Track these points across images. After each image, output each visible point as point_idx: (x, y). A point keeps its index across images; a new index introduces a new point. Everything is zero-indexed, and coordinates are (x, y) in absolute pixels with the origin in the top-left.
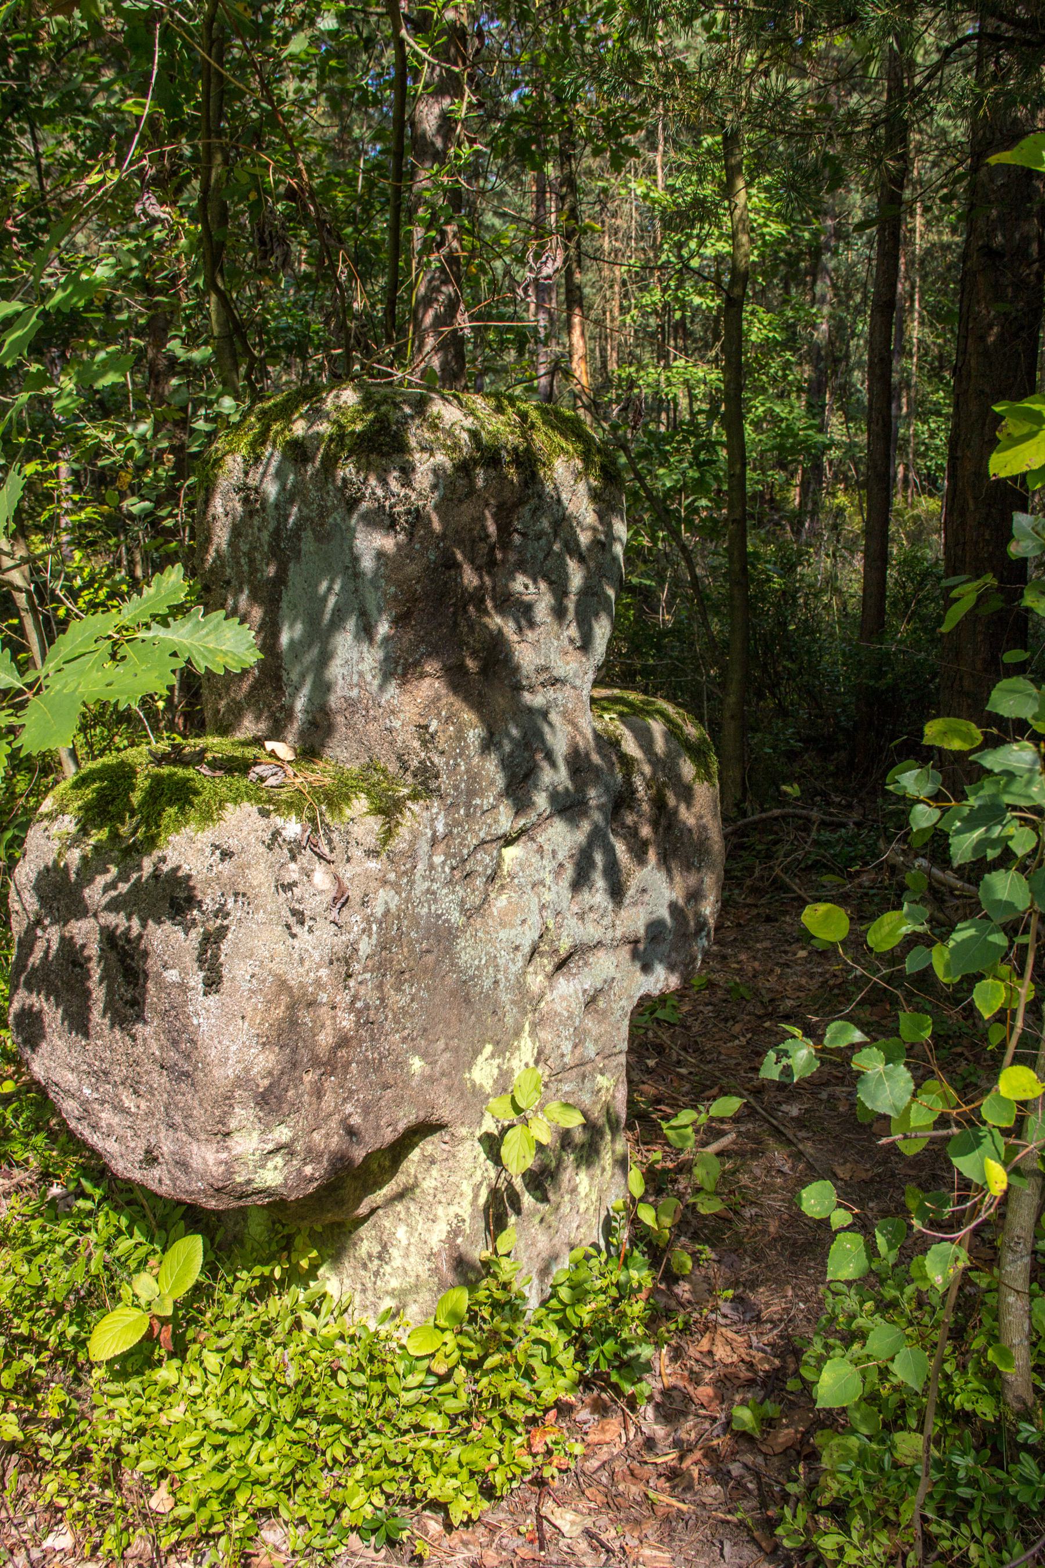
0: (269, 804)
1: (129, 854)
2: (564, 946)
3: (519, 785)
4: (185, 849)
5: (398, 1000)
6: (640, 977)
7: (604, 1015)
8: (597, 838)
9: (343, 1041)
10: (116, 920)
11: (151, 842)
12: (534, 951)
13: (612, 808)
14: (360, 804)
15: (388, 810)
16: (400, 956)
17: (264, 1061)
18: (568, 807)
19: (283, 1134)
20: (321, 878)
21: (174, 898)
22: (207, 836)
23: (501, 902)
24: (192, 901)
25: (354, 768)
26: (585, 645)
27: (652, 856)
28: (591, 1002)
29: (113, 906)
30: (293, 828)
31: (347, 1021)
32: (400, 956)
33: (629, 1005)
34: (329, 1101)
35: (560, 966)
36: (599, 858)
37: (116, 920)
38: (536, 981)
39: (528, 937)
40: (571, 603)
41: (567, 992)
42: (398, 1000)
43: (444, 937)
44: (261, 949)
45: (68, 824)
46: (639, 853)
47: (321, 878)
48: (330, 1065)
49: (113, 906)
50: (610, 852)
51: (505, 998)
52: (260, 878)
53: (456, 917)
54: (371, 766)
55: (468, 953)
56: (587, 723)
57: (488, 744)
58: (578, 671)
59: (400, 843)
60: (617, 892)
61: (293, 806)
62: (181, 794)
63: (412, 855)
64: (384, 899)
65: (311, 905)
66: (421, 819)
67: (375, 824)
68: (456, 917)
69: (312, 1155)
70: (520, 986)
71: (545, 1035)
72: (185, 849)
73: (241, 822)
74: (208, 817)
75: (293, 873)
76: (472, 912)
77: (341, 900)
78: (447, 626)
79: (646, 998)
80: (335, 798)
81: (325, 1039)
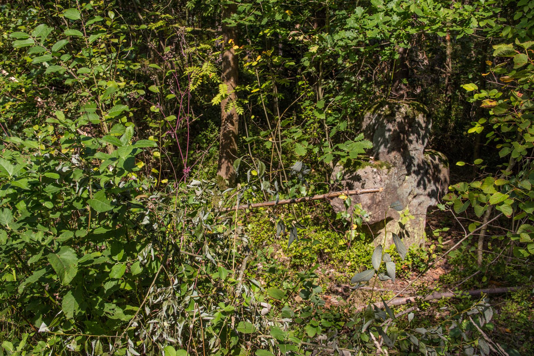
0: (372, 166)
1: (352, 172)
2: (415, 193)
3: (409, 168)
4: (360, 172)
5: (388, 197)
6: (429, 202)
7: (422, 207)
8: (422, 179)
9: (380, 201)
10: (349, 181)
11: (355, 171)
12: (410, 194)
13: (425, 173)
14: (385, 167)
15: (389, 168)
16: (389, 190)
17: (369, 202)
18: (417, 173)
19: (370, 213)
20: (379, 177)
21: (358, 178)
22: (363, 170)
23: (405, 184)
24: (361, 179)
25: (383, 162)
26: (423, 144)
27: (432, 182)
28: (420, 204)
29: (349, 179)
30: (375, 170)
31: (381, 198)
32: (389, 190)
33: (427, 206)
34: (377, 210)
35: (415, 197)
36: (422, 182)
37: (349, 181)
38: (410, 198)
39: (409, 191)
40: (421, 137)
41: (415, 202)
42: (388, 197)
43: (395, 188)
44: (370, 187)
45: (342, 167)
46: (429, 181)
47: (379, 177)
48: (377, 204)
49: (349, 179)
50: (424, 181)
51: (404, 200)
52: (370, 176)
53: (397, 186)
54: (386, 162)
55: (399, 191)
56: (423, 157)
57: (404, 163)
58: (420, 147)
59: (390, 173)
60: (425, 188)
61: (375, 167)
62: (359, 164)
63: (392, 175)
64: (387, 181)
65: (377, 181)
66: (393, 170)
67: (387, 170)
68: (397, 186)
69: (374, 218)
70: (407, 199)
71: (411, 208)
72: (360, 172)
73: (368, 168)
74: (363, 167)
75: (375, 176)
76: (401, 185)
77: (381, 181)
78: (399, 144)
79: (430, 206)
80: (381, 166)
81: (377, 200)
